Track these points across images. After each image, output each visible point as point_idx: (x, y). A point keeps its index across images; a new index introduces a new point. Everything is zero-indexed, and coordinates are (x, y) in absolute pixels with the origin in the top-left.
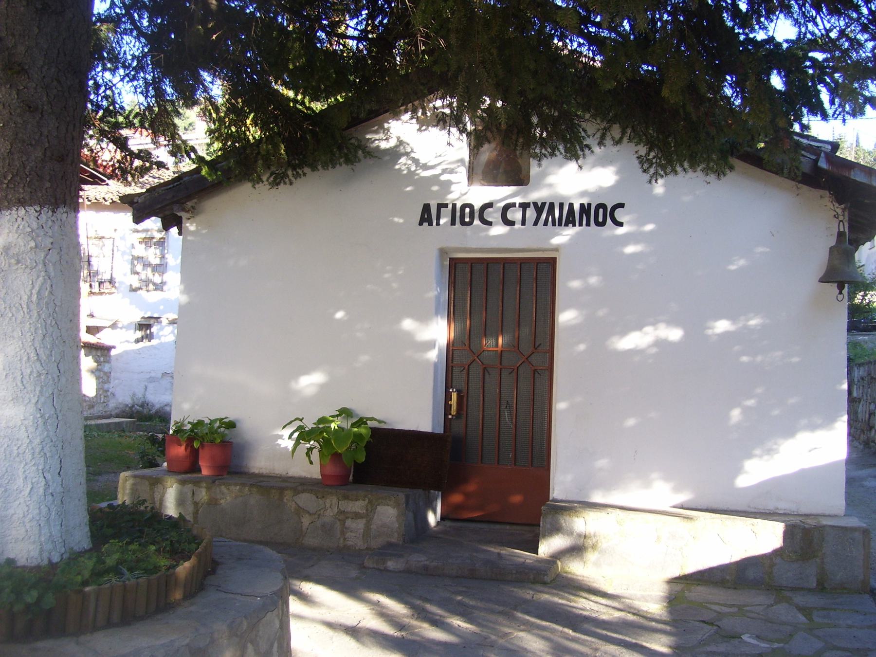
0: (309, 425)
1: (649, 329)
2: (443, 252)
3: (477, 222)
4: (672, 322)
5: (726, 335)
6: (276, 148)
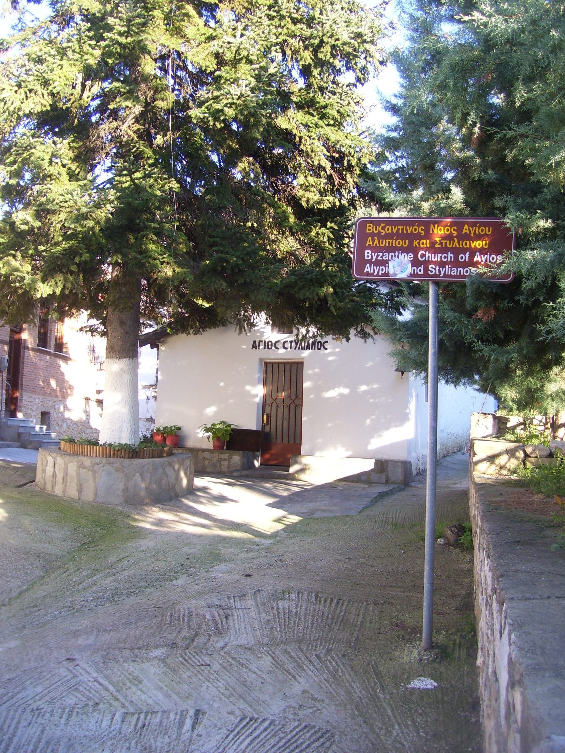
0: (209, 426)
1: (336, 389)
2: (261, 360)
3: (273, 348)
4: (345, 386)
5: (365, 392)
6: (195, 323)
